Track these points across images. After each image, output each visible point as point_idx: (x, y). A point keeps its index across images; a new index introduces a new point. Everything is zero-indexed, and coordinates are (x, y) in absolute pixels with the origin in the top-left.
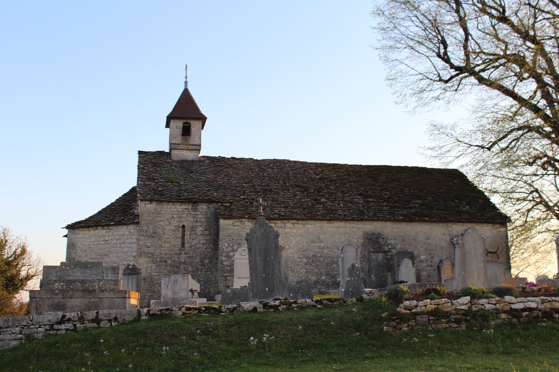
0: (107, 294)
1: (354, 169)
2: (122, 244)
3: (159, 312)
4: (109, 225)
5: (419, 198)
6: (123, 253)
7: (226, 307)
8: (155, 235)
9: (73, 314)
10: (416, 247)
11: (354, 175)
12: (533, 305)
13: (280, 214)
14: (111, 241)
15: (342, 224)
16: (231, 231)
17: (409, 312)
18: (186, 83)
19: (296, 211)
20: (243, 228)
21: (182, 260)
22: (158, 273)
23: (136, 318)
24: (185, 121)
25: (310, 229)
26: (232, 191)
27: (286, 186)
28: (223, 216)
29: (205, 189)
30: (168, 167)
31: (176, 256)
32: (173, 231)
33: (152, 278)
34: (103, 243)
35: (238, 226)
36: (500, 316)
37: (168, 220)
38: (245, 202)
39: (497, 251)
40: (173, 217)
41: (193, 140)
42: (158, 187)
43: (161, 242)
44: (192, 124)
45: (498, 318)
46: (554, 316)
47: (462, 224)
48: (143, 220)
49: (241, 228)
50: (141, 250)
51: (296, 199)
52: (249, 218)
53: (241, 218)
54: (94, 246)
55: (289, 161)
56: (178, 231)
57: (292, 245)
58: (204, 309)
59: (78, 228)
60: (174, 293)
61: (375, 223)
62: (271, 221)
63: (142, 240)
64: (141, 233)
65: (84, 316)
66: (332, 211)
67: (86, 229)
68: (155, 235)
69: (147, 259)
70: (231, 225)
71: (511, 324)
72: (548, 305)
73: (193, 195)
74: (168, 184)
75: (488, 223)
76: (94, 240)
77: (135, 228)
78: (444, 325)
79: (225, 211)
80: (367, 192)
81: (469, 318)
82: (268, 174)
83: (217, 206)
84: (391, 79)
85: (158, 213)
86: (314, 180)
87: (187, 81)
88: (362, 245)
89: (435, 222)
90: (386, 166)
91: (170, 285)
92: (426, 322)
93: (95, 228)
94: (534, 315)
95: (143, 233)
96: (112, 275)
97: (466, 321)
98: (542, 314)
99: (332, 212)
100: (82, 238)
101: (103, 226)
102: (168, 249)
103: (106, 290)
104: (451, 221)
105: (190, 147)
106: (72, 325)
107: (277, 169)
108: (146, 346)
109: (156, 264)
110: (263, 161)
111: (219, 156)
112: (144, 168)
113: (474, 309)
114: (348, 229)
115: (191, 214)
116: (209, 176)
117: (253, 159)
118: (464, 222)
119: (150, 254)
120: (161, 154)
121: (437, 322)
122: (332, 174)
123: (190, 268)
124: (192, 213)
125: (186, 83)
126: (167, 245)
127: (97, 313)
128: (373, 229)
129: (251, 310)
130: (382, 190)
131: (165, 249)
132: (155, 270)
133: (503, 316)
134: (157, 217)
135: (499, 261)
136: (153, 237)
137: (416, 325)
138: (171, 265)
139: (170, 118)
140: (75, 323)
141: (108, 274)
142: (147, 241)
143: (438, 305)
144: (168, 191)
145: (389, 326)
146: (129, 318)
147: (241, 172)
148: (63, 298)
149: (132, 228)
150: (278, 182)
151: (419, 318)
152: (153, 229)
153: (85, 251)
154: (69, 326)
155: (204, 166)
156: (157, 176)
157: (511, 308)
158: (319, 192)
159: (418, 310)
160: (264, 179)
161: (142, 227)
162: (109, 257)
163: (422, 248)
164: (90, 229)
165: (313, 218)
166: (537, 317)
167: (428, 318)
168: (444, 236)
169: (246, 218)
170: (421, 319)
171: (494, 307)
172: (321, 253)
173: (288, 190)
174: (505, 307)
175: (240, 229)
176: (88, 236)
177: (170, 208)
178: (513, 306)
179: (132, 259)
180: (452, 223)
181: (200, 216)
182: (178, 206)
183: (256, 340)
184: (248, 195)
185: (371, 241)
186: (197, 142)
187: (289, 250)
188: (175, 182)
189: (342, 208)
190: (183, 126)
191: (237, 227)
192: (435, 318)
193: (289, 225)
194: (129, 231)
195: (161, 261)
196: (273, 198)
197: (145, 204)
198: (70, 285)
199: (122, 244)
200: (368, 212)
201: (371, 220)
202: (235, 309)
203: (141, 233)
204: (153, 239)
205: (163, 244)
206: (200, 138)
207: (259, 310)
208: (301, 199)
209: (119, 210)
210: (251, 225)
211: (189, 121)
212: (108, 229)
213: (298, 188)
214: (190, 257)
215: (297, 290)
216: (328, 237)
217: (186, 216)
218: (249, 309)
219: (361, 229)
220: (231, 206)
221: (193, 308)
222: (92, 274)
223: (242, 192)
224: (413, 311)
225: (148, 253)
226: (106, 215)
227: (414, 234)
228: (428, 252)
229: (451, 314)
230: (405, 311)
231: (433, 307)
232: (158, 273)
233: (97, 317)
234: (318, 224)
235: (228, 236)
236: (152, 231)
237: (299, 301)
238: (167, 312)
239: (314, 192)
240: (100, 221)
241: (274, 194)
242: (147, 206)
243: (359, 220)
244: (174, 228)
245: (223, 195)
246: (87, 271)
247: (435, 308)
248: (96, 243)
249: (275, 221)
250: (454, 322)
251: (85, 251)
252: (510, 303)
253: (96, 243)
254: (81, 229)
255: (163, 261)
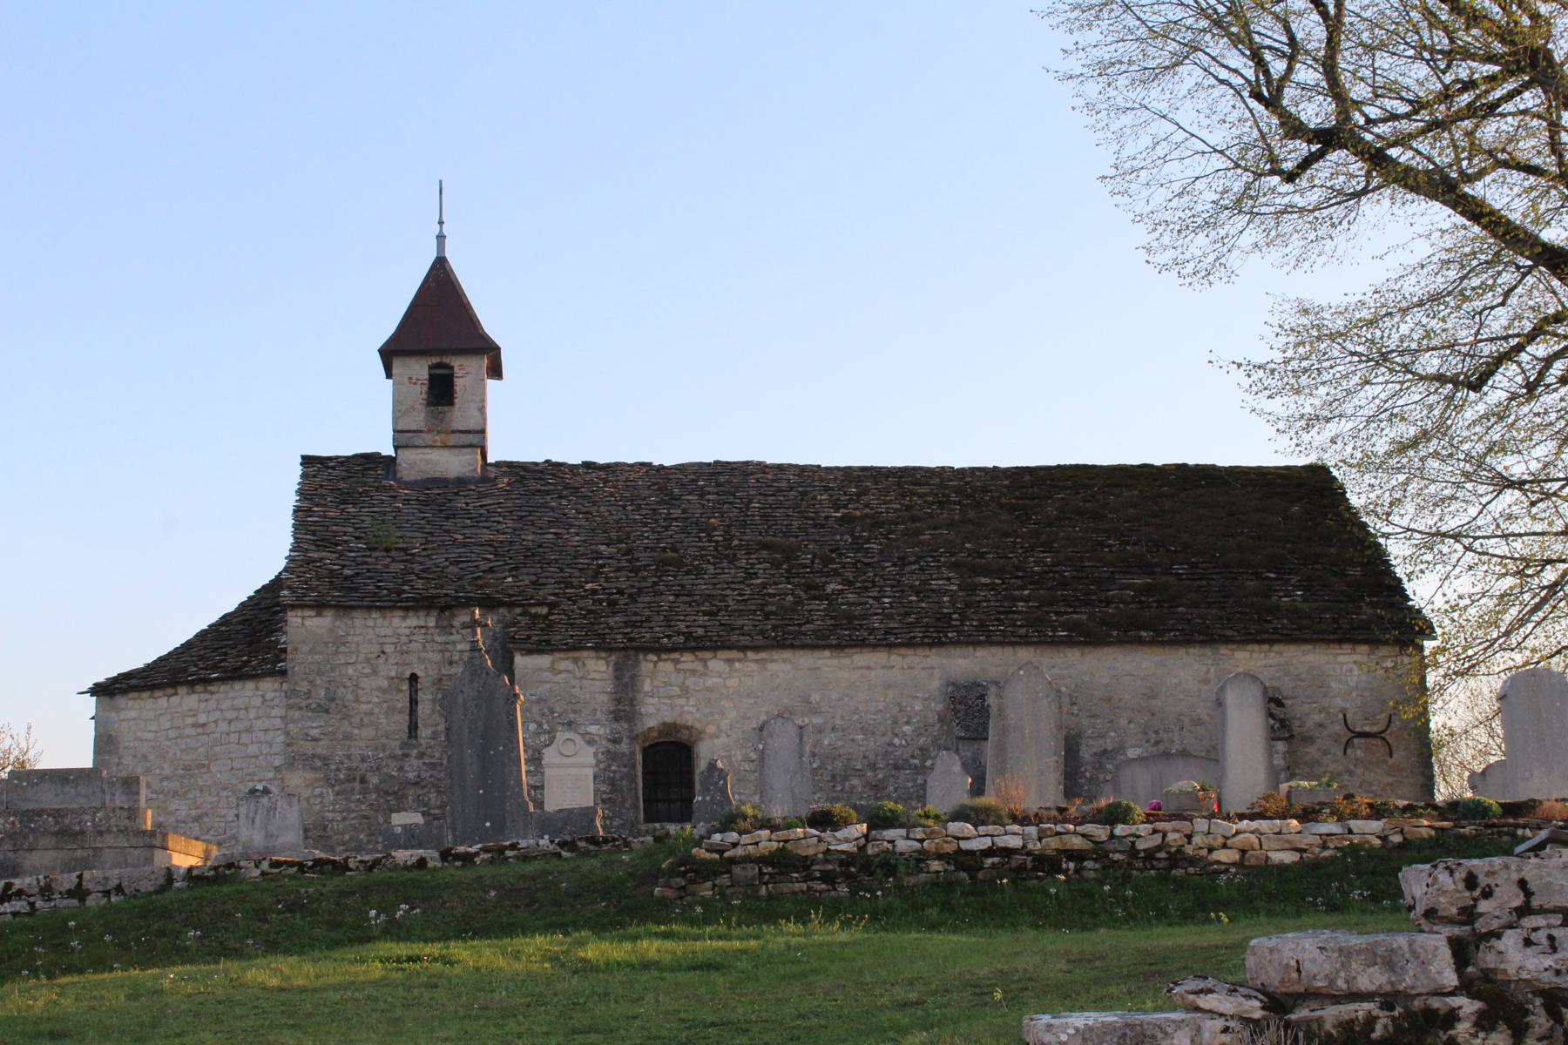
0: (109, 840)
1: (967, 483)
2: (243, 735)
3: (212, 873)
4: (206, 681)
5: (1147, 568)
6: (248, 760)
7: (359, 858)
8: (333, 706)
9: (28, 880)
10: (1111, 721)
11: (959, 503)
12: (1015, 842)
13: (691, 633)
14: (213, 725)
15: (878, 658)
16: (547, 686)
17: (717, 856)
18: (441, 238)
19: (740, 622)
20: (582, 678)
21: (411, 775)
22: (341, 812)
23: (162, 886)
24: (435, 360)
25: (781, 675)
26: (562, 570)
27: (729, 547)
28: (523, 646)
29: (482, 568)
30: (383, 502)
31: (393, 764)
32: (384, 691)
33: (325, 828)
34: (193, 731)
35: (568, 671)
36: (928, 866)
37: (368, 660)
38: (594, 601)
39: (1384, 731)
40: (383, 652)
41: (460, 416)
42: (344, 567)
43: (350, 723)
44: (456, 370)
45: (921, 871)
46: (1064, 866)
47: (1266, 647)
48: (300, 661)
49: (575, 677)
50: (294, 748)
51: (749, 585)
52: (596, 648)
53: (574, 648)
54: (168, 743)
55: (762, 467)
56: (400, 691)
57: (725, 723)
58: (310, 863)
59: (124, 692)
60: (268, 836)
61: (981, 652)
62: (663, 656)
63: (294, 722)
64: (291, 701)
65: (53, 885)
66: (850, 618)
67: (146, 695)
68: (333, 706)
69: (310, 775)
70: (547, 670)
71: (949, 885)
72: (1053, 843)
73: (442, 587)
74: (375, 554)
75: (1355, 642)
76: (168, 725)
77: (277, 686)
78: (797, 885)
79: (530, 629)
80: (982, 556)
81: (853, 869)
82: (684, 511)
83: (509, 617)
84: (1122, 175)
85: (340, 642)
86: (823, 526)
87: (445, 233)
88: (941, 720)
89: (1171, 643)
90: (1077, 467)
91: (258, 817)
92: (753, 878)
93: (170, 691)
94: (1014, 864)
95: (297, 700)
96: (124, 798)
97: (849, 877)
98: (1033, 861)
99: (850, 623)
100: (134, 719)
101: (192, 684)
102: (370, 743)
103: (109, 831)
104: (1227, 641)
105: (453, 439)
106: (25, 903)
107: (717, 494)
108: (162, 933)
109: (337, 788)
110: (681, 468)
111: (547, 461)
112: (310, 510)
113: (870, 852)
114: (895, 671)
115: (433, 641)
116: (501, 527)
117: (649, 465)
118: (1271, 642)
119: (320, 758)
120: (369, 461)
121: (778, 878)
122: (890, 502)
123: (433, 796)
124: (438, 639)
125: (441, 238)
126: (368, 733)
127: (80, 877)
128: (977, 669)
129: (413, 866)
130: (1032, 548)
131: (361, 744)
132: (334, 805)
133: (936, 865)
134: (336, 653)
135: (1391, 761)
136: (327, 711)
137: (732, 886)
138: (377, 790)
139: (390, 354)
140: (32, 899)
141: (113, 795)
142: (309, 724)
143: (786, 841)
144: (370, 578)
145: (669, 887)
146: (147, 886)
147: (602, 509)
148: (15, 851)
149: (268, 686)
150: (709, 535)
151: (737, 870)
152: (328, 689)
153: (145, 757)
154: (20, 905)
155: (492, 495)
156: (345, 534)
157: (959, 849)
158: (826, 560)
159: (739, 852)
160: (666, 528)
161: (296, 683)
162: (209, 771)
163: (1132, 726)
164: (158, 693)
165: (789, 642)
166: (1021, 868)
167: (760, 869)
168: (1204, 687)
169: (589, 648)
170: (743, 873)
171: (917, 845)
172: (815, 746)
173: (733, 559)
174: (945, 846)
175: (573, 682)
176: (151, 714)
177: (373, 628)
178: (964, 845)
179: (271, 775)
180: (1231, 646)
181: (460, 647)
182: (396, 621)
183: (383, 917)
184: (607, 580)
185: (962, 707)
186: (473, 421)
187: (718, 737)
188: (396, 549)
189: (884, 609)
190: (430, 375)
191: (564, 675)
192: (776, 870)
193: (717, 664)
194: (263, 697)
195: (350, 779)
196: (683, 586)
197: (303, 618)
198: (30, 821)
199: (243, 735)
200: (963, 618)
201: (968, 644)
202: (377, 862)
203: (291, 701)
204: (325, 715)
205: (356, 731)
206: (482, 410)
207: (431, 864)
208: (764, 586)
209: (240, 636)
210: (603, 668)
211: (446, 360)
212: (206, 691)
213: (765, 554)
214: (433, 766)
215: (559, 825)
216: (834, 696)
217: (421, 647)
218: (409, 863)
219: (937, 672)
220: (550, 613)
221: (285, 862)
222: (78, 794)
223: (590, 572)
224: (726, 854)
225: (314, 756)
226: (202, 652)
227: (1105, 681)
228: (1153, 737)
229: (814, 861)
230: (708, 855)
231: (775, 845)
232: (341, 812)
233: (79, 885)
234: (806, 659)
235: (539, 701)
236: (322, 693)
237: (523, 844)
238: (228, 872)
239: (813, 562)
240: (185, 670)
241: (688, 573)
242: (307, 623)
243: (931, 645)
244: (385, 684)
245: (533, 583)
246: (67, 788)
247: (778, 849)
248: (172, 734)
249: (676, 655)
250: (817, 879)
251: (145, 757)
252: (958, 838)
253: (172, 734)
254: (131, 695)
255: (354, 779)
